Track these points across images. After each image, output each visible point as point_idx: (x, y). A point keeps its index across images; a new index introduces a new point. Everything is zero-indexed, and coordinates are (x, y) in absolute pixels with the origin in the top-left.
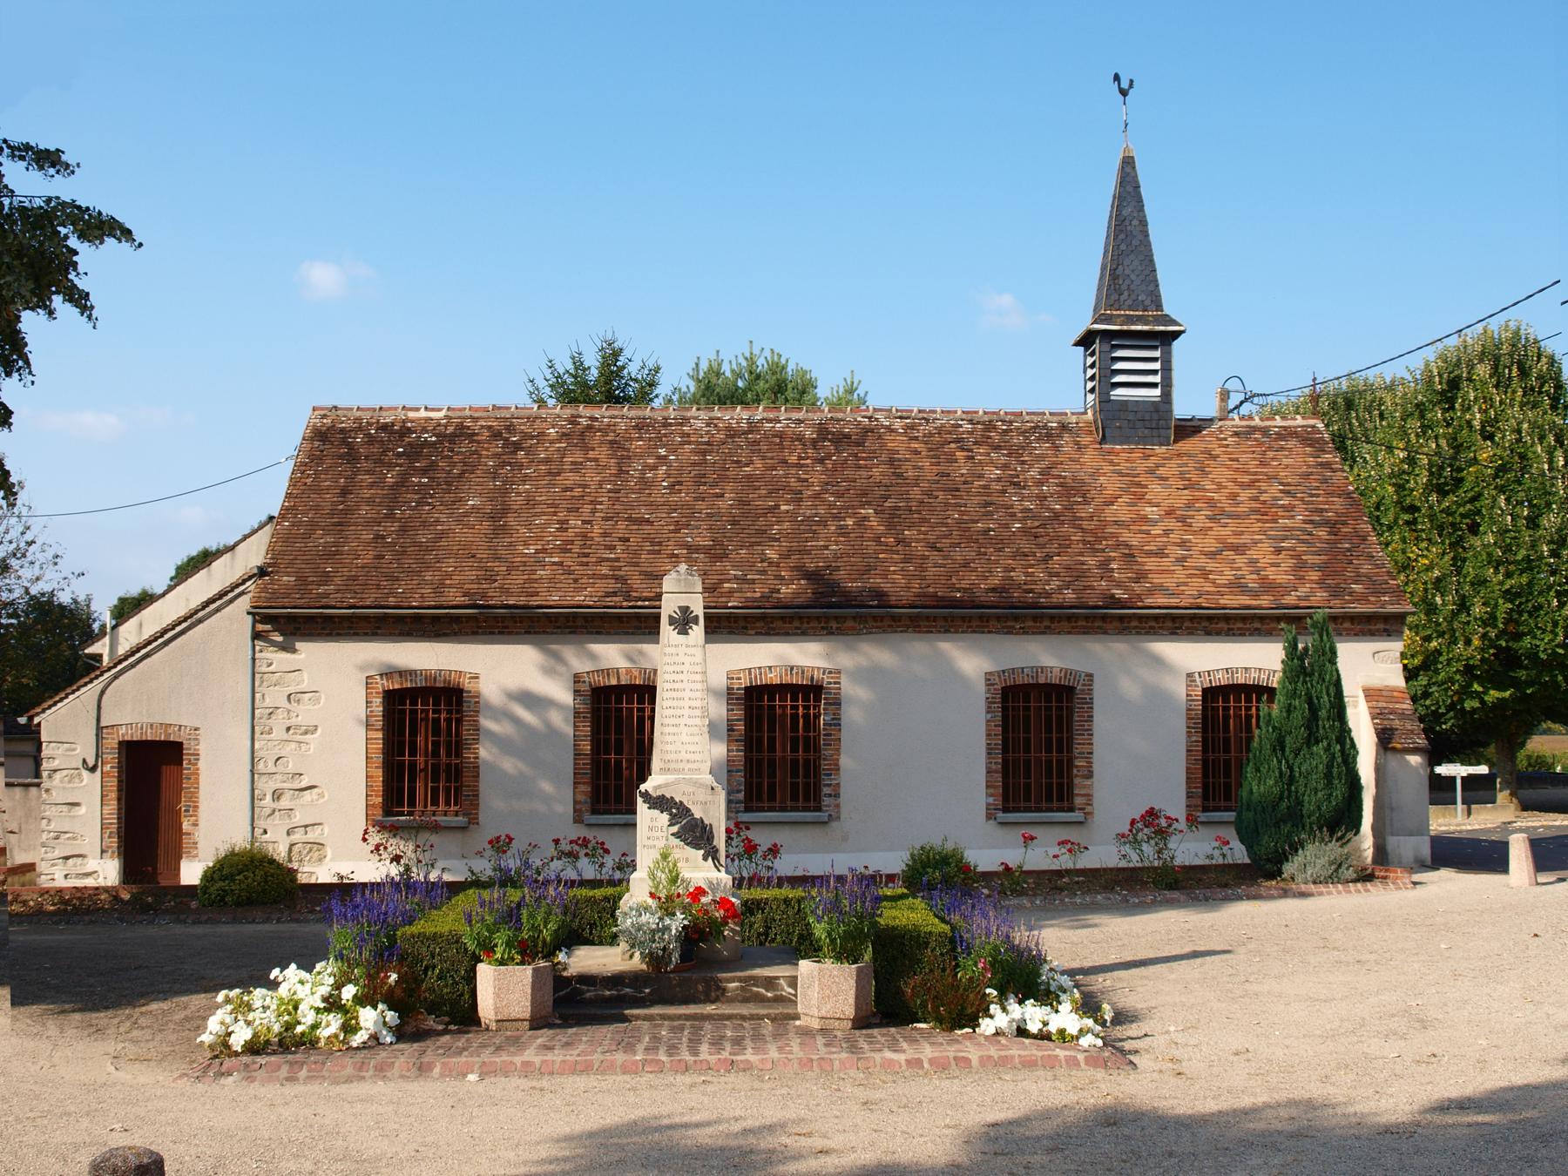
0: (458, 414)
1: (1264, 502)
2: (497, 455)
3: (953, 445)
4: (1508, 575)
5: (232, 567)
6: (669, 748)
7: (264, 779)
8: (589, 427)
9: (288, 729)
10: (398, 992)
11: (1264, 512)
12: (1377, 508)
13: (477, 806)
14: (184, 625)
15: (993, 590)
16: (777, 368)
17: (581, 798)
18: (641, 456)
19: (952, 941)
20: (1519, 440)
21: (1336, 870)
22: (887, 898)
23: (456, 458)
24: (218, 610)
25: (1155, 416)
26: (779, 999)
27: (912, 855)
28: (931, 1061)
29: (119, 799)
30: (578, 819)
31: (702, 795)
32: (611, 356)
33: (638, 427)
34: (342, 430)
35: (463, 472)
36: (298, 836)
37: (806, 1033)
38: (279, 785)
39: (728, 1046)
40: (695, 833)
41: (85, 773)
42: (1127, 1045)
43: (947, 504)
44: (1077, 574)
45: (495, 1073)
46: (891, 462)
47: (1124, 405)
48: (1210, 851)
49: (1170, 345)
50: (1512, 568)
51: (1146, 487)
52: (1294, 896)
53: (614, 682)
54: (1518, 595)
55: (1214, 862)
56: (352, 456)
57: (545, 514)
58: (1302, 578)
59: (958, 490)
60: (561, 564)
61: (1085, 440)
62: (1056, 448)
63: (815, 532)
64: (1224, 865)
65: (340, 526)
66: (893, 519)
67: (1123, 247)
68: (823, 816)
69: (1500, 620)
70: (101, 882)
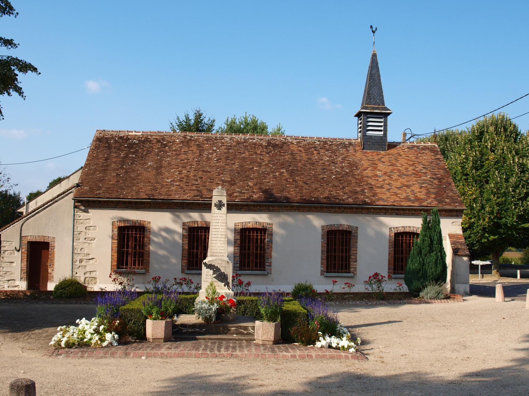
0: (146, 134)
1: (417, 171)
3: (313, 149)
4: (498, 198)
6: (213, 248)
7: (77, 255)
8: (190, 140)
9: (85, 239)
10: (119, 328)
11: (417, 174)
12: (455, 174)
13: (149, 267)
14: (51, 203)
15: (325, 198)
19: (307, 315)
20: (503, 153)
21: (438, 295)
22: (286, 301)
24: (62, 198)
25: (381, 141)
26: (249, 334)
27: (295, 287)
28: (299, 356)
29: (27, 261)
30: (183, 272)
31: (224, 264)
33: (207, 140)
34: (106, 138)
35: (147, 153)
36: (88, 275)
37: (257, 345)
38: (82, 258)
39: (231, 349)
40: (222, 277)
41: (16, 252)
43: (310, 169)
46: (292, 154)
47: (371, 137)
49: (387, 117)
50: (499, 195)
51: (377, 165)
53: (196, 226)
54: (501, 204)
55: (397, 291)
56: (109, 147)
57: (174, 168)
60: (179, 185)
61: (357, 148)
62: (348, 151)
63: (265, 177)
65: (105, 170)
66: (292, 173)
67: (372, 84)
68: (266, 273)
70: (20, 289)
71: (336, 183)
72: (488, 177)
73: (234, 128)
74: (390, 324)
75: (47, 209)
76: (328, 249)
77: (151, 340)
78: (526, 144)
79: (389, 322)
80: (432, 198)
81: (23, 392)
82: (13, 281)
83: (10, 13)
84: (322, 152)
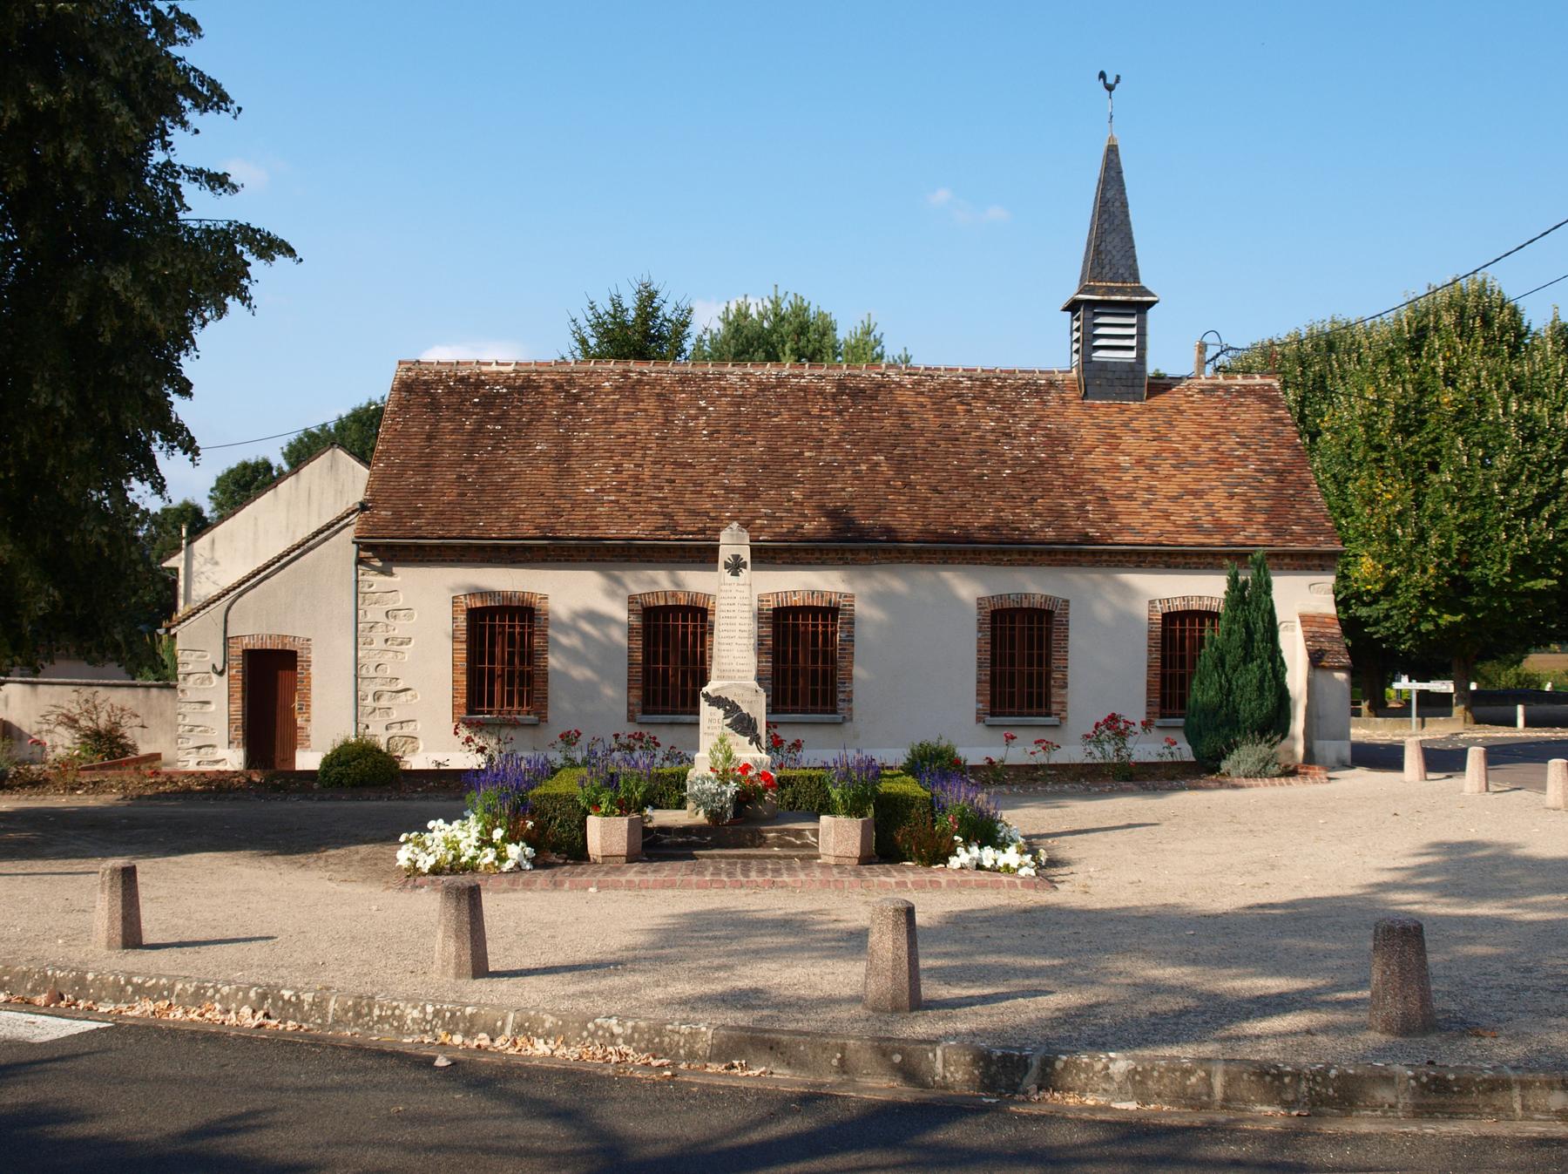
0: (525, 368)
1: (1222, 453)
2: (559, 406)
3: (954, 400)
4: (1463, 510)
5: (297, 488)
6: (724, 660)
7: (366, 682)
8: (639, 381)
9: (387, 640)
10: (534, 836)
11: (1222, 461)
12: (1349, 446)
13: (546, 707)
14: (297, 552)
15: (985, 528)
16: (800, 310)
17: (634, 700)
18: (684, 407)
19: (932, 802)
20: (1478, 386)
21: (1264, 767)
22: (887, 776)
23: (525, 408)
24: (326, 539)
25: (1131, 376)
26: (805, 846)
27: (912, 751)
28: (913, 883)
29: (243, 699)
30: (631, 718)
31: (749, 696)
32: (648, 298)
33: (681, 382)
34: (425, 382)
35: (531, 421)
36: (395, 731)
37: (825, 866)
38: (378, 688)
39: (770, 874)
40: (744, 724)
41: (214, 677)
42: (1056, 879)
43: (947, 452)
44: (1059, 514)
45: (607, 887)
46: (900, 414)
47: (1104, 365)
48: (1161, 751)
49: (1145, 313)
50: (1467, 503)
51: (1120, 438)
52: (1228, 788)
53: (662, 603)
54: (1471, 528)
55: (1164, 759)
56: (435, 406)
57: (602, 458)
58: (1250, 520)
59: (957, 440)
60: (617, 502)
61: (1069, 395)
62: (1044, 402)
63: (833, 476)
64: (1173, 763)
65: (428, 465)
66: (900, 465)
67: (1106, 226)
68: (838, 718)
69: (1454, 551)
70: (229, 767)
71: (1014, 489)
72: (1436, 453)
73: (745, 332)
74: (1129, 830)
75: (287, 569)
76: (993, 655)
77: (600, 860)
78: (1542, 360)
79: (1129, 826)
80: (1259, 523)
81: (466, 897)
82: (210, 750)
83: (220, 108)
84: (978, 408)
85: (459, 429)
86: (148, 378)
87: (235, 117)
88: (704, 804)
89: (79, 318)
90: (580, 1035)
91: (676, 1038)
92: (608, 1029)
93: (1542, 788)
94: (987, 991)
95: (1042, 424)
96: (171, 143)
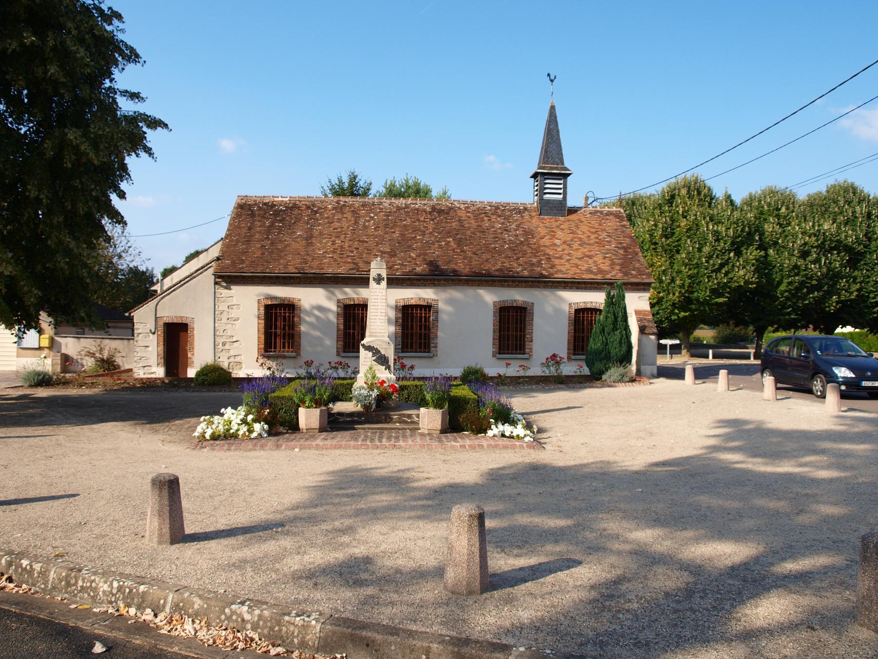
2: (308, 215)
4: (690, 269)
8: (344, 205)
10: (269, 418)
11: (600, 243)
12: (642, 243)
13: (300, 349)
15: (497, 270)
19: (478, 401)
20: (696, 219)
23: (293, 216)
24: (201, 273)
26: (413, 422)
28: (469, 446)
29: (164, 345)
30: (338, 354)
31: (385, 345)
32: (353, 178)
33: (363, 206)
34: (249, 205)
36: (232, 360)
37: (422, 435)
39: (393, 440)
40: (382, 360)
41: (151, 335)
42: (542, 441)
43: (480, 237)
45: (305, 448)
47: (548, 201)
53: (352, 303)
54: (693, 277)
56: (253, 215)
60: (332, 257)
61: (533, 214)
62: (522, 217)
65: (248, 241)
66: (459, 243)
68: (431, 355)
71: (510, 254)
74: (570, 410)
76: (500, 327)
79: (569, 408)
81: (166, 487)
85: (263, 225)
86: (93, 187)
87: (143, 66)
88: (361, 401)
89: (52, 153)
90: (219, 618)
91: (292, 628)
92: (240, 615)
93: (717, 382)
94: (533, 561)
95: (522, 226)
96: (114, 79)
